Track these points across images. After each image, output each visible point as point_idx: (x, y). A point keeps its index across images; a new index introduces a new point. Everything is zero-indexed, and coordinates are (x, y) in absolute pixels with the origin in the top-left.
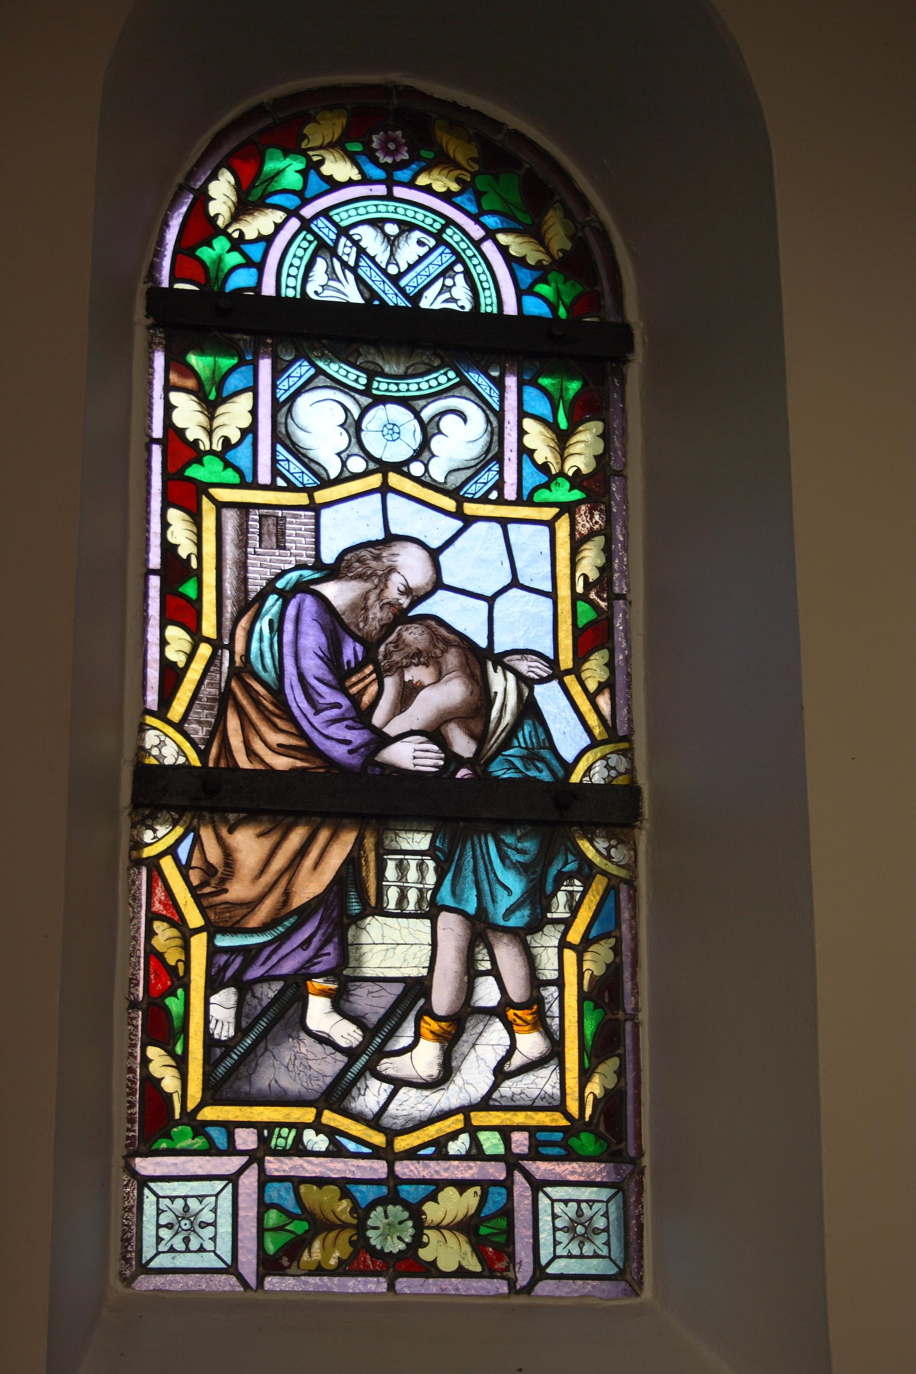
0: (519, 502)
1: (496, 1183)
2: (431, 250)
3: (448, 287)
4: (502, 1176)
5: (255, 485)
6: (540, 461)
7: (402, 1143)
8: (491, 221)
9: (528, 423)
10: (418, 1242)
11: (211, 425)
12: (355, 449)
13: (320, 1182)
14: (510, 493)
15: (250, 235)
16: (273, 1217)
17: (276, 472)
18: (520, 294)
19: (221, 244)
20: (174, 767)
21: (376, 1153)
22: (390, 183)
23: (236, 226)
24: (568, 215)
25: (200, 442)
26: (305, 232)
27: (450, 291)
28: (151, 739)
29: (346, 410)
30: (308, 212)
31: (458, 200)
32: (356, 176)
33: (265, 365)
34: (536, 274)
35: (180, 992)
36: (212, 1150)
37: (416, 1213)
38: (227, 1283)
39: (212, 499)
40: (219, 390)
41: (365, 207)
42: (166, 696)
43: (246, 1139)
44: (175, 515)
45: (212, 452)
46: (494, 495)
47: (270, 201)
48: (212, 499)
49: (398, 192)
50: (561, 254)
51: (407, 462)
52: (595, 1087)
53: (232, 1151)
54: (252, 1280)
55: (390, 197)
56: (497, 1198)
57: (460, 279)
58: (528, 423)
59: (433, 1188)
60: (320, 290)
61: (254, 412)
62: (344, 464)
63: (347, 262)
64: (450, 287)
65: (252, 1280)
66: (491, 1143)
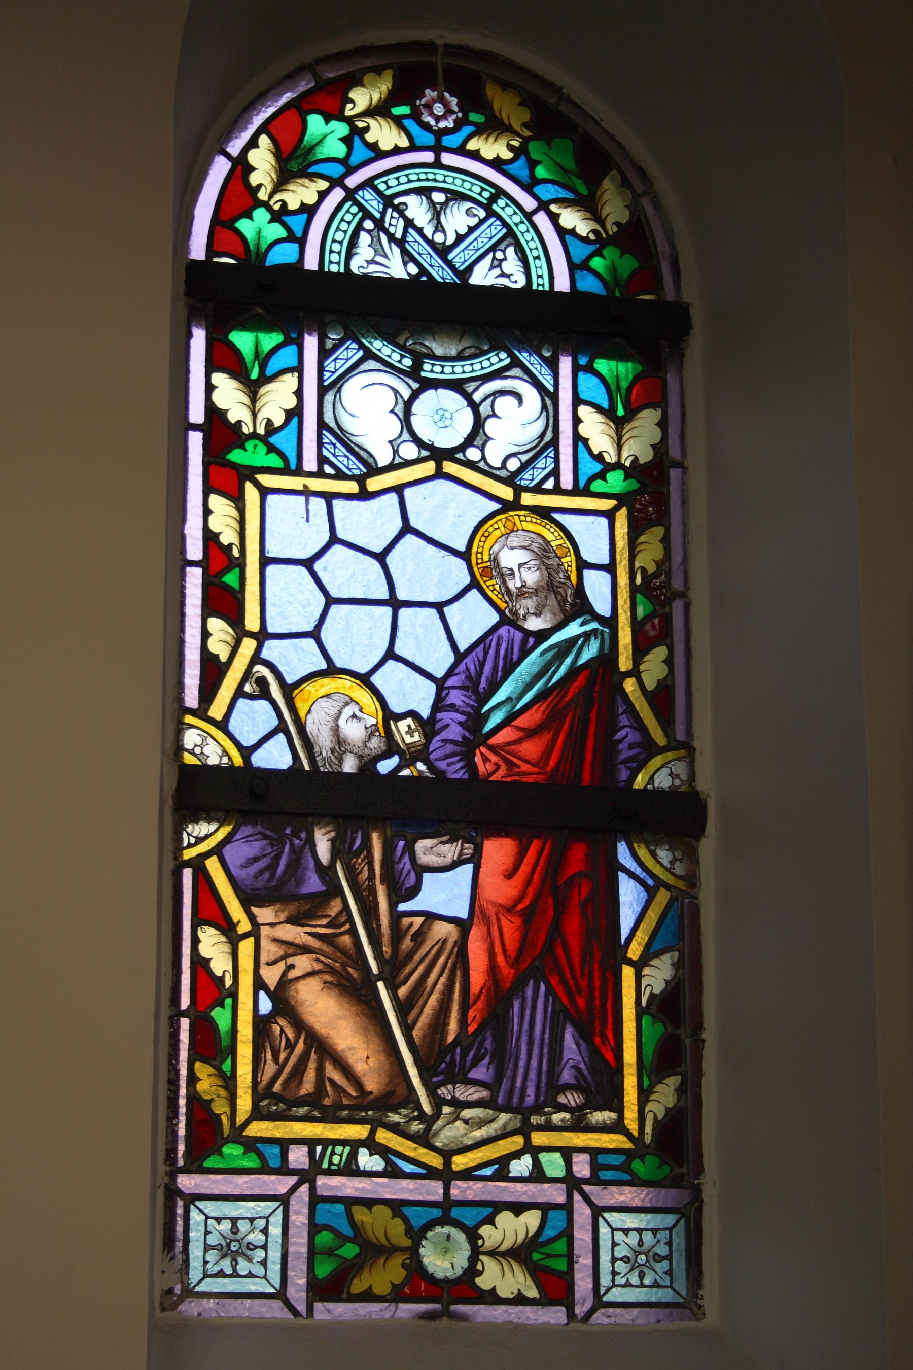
0: (576, 491)
1: (556, 1206)
2: (481, 222)
3: (498, 260)
4: (561, 1199)
5: (299, 472)
6: (596, 452)
7: (460, 1162)
8: (546, 192)
9: (583, 410)
10: (472, 1271)
11: (254, 407)
12: (406, 436)
13: (369, 1203)
14: (567, 481)
15: (293, 205)
16: (325, 1238)
17: (322, 460)
18: (573, 267)
19: (261, 215)
20: (217, 768)
21: (430, 1173)
22: (438, 149)
23: (278, 197)
24: (625, 183)
25: (243, 423)
26: (350, 203)
27: (499, 266)
28: (191, 738)
29: (396, 392)
30: (352, 181)
31: (510, 168)
32: (404, 142)
33: (311, 343)
34: (591, 248)
35: (229, 1001)
36: (265, 1169)
37: (473, 1236)
38: (276, 1311)
39: (257, 485)
40: (263, 368)
41: (407, 175)
42: (208, 692)
43: (298, 1157)
44: (217, 502)
45: (254, 435)
46: (549, 484)
47: (313, 169)
48: (257, 485)
49: (447, 159)
50: (615, 229)
51: (462, 448)
52: (657, 1108)
53: (284, 1170)
54: (302, 1308)
55: (437, 164)
56: (557, 1220)
57: (510, 251)
58: (583, 410)
59: (490, 1210)
60: (365, 265)
61: (299, 393)
62: (396, 452)
63: (393, 235)
64: (501, 261)
65: (302, 1308)
66: (553, 1164)
